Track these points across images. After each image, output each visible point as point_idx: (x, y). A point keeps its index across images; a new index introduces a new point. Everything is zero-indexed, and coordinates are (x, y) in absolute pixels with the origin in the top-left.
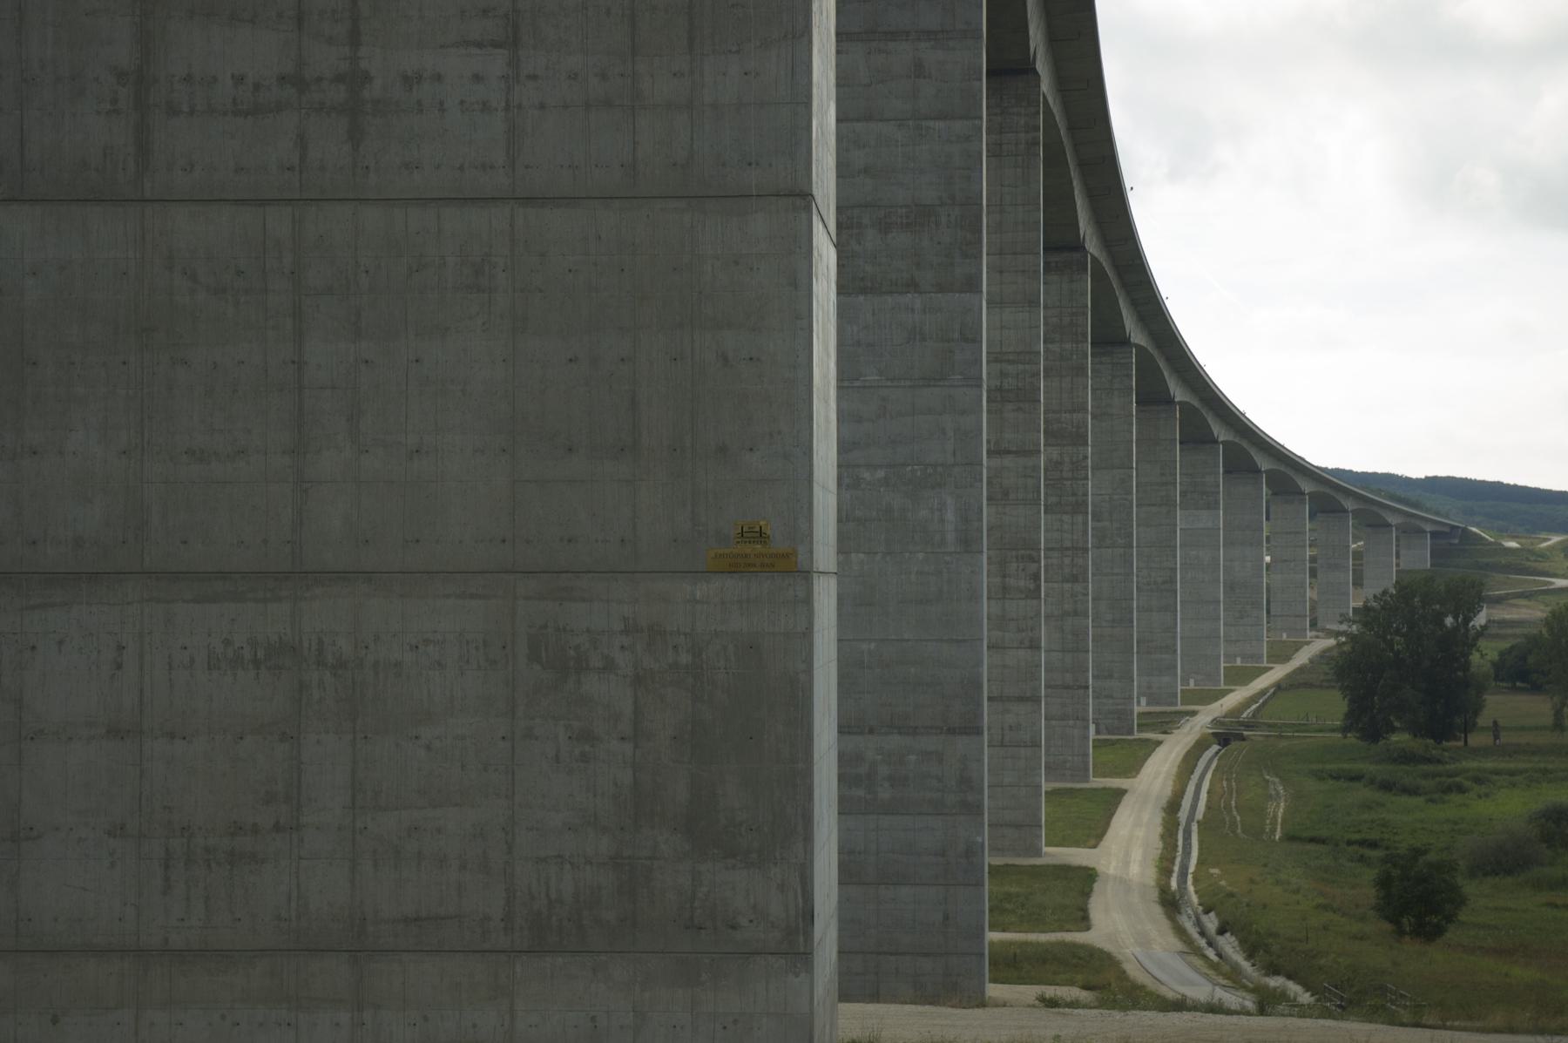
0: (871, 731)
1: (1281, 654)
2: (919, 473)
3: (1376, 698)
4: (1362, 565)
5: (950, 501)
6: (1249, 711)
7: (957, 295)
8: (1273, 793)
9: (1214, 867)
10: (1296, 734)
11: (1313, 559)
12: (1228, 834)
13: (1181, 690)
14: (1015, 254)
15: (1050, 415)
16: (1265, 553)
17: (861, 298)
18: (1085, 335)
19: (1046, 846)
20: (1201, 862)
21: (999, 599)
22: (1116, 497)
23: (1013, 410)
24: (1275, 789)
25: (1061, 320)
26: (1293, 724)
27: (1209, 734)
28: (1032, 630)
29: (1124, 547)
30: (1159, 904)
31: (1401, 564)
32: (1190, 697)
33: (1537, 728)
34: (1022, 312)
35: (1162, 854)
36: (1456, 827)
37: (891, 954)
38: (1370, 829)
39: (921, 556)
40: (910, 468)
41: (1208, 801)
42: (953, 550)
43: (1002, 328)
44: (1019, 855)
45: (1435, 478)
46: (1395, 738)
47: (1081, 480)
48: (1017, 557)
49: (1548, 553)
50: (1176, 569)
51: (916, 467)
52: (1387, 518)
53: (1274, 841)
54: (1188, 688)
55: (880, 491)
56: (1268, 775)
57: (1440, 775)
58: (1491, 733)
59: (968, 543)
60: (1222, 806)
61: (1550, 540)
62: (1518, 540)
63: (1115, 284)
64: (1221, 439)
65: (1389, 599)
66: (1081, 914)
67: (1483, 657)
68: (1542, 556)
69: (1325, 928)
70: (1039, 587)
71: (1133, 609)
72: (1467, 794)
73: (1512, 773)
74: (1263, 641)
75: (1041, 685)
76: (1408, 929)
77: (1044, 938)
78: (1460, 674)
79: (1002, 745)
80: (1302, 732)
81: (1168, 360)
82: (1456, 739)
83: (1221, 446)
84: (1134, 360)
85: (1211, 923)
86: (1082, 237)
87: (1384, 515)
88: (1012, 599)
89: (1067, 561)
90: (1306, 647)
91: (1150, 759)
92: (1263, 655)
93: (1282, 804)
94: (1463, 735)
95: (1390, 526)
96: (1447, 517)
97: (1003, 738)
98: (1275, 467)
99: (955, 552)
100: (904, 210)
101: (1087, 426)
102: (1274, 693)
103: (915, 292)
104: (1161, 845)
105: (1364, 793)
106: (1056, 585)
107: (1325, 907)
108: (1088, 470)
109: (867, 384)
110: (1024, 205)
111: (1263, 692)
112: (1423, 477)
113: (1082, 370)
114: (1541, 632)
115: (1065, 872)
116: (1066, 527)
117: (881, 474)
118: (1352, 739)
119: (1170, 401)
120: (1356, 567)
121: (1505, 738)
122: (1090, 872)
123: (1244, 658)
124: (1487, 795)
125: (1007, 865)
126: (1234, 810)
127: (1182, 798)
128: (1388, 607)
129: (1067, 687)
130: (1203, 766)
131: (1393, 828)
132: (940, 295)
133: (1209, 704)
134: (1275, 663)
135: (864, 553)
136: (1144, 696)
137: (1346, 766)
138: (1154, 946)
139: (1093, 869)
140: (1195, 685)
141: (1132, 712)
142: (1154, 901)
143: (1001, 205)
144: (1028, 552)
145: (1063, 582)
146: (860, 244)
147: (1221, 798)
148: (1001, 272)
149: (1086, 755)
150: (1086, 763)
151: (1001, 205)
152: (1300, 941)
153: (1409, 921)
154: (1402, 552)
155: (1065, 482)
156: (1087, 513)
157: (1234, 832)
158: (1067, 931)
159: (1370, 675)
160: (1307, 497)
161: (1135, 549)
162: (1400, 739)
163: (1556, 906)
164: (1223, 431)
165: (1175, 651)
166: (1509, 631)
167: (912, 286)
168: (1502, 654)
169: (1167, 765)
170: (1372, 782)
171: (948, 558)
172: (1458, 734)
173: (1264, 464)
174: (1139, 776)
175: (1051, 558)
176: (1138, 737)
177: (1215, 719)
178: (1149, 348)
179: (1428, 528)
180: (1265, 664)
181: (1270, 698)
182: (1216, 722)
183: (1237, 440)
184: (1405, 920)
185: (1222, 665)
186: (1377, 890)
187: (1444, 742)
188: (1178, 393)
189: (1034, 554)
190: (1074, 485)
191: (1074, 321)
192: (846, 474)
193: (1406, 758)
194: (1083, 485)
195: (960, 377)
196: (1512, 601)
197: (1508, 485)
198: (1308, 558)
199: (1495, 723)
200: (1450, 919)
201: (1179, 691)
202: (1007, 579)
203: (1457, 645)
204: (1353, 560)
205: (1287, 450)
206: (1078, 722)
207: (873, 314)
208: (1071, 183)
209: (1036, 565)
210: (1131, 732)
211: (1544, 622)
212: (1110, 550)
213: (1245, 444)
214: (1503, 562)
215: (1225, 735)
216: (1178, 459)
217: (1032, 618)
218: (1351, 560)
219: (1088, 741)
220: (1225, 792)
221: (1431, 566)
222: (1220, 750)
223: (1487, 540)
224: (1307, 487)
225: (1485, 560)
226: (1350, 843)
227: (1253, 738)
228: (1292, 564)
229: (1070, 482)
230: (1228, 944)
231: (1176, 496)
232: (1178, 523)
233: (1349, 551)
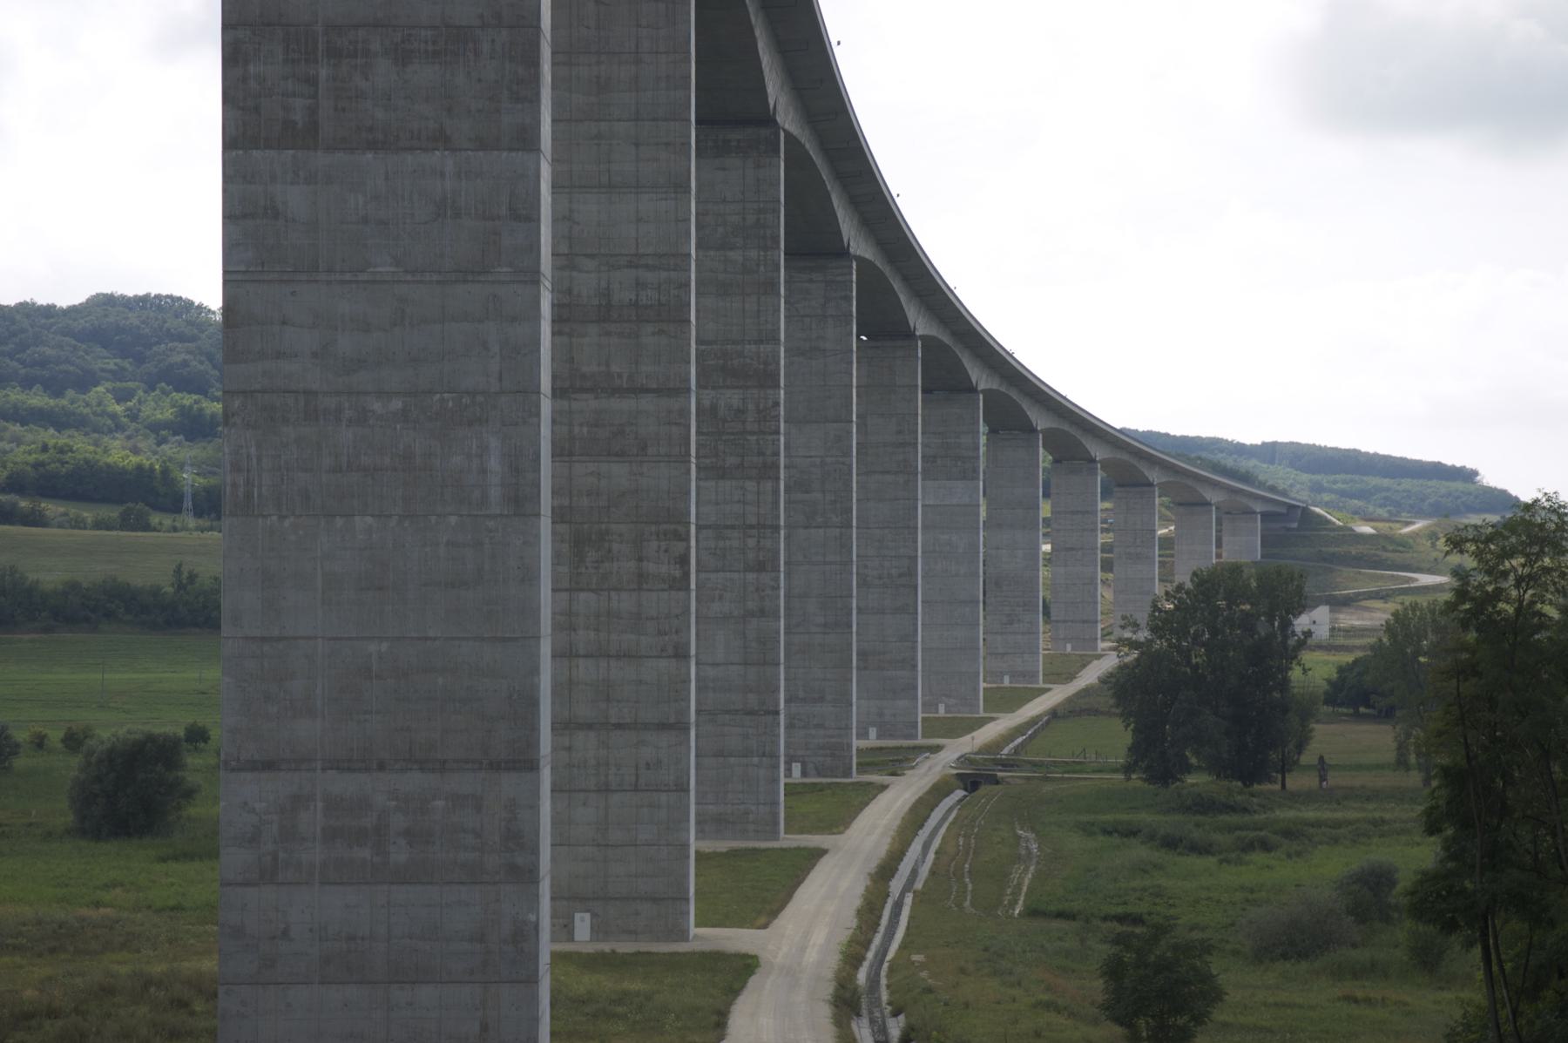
0: (382, 767)
1: (1061, 672)
2: (450, 404)
3: (1167, 727)
4: (1172, 556)
5: (494, 443)
6: (1011, 746)
12: (951, 907)
14: (654, 120)
16: (1041, 541)
17: (370, 156)
18: (776, 239)
19: (697, 925)
20: (904, 946)
21: (634, 590)
22: (829, 460)
23: (653, 334)
24: (1027, 848)
25: (744, 219)
27: (953, 775)
28: (677, 632)
30: (831, 1003)
31: (1224, 554)
32: (933, 727)
34: (666, 199)
36: (1250, 897)
38: (1140, 899)
39: (453, 520)
40: (438, 396)
41: (934, 864)
42: (498, 512)
43: (639, 220)
45: (1274, 444)
46: (1191, 779)
47: (771, 434)
49: (1411, 541)
51: (446, 395)
52: (1205, 495)
53: (1012, 917)
54: (936, 715)
55: (395, 428)
56: (1021, 830)
57: (1240, 828)
58: (1317, 774)
59: (521, 502)
60: (952, 869)
61: (1413, 523)
64: (981, 387)
65: (1185, 596)
66: (714, 1018)
68: (1403, 544)
70: (687, 575)
72: (1273, 854)
73: (1337, 825)
74: (1039, 653)
76: (1144, 1034)
79: (636, 790)
80: (1074, 772)
81: (905, 279)
82: (1271, 780)
89: (751, 542)
90: (1095, 662)
93: (1032, 868)
94: (1280, 776)
95: (1208, 504)
97: (637, 781)
99: (501, 515)
100: (429, 33)
102: (1048, 722)
103: (446, 149)
104: (854, 923)
105: (1139, 851)
106: (736, 576)
107: (1048, 1006)
111: (1033, 722)
112: (1259, 443)
113: (772, 286)
114: (1380, 640)
119: (909, 335)
120: (1165, 559)
121: (1334, 779)
122: (750, 961)
123: (1014, 675)
124: (1299, 854)
125: (639, 953)
126: (966, 875)
128: (1183, 607)
131: (1170, 898)
132: (481, 153)
135: (372, 516)
136: (875, 726)
137: (1124, 817)
140: (946, 712)
141: (850, 746)
144: (672, 527)
145: (745, 571)
146: (367, 79)
147: (952, 861)
148: (637, 145)
149: (776, 803)
150: (775, 815)
151: (637, 53)
153: (1147, 1023)
154: (1225, 539)
155: (749, 437)
156: (778, 479)
157: (960, 905)
161: (854, 530)
162: (1197, 781)
163: (1356, 1001)
164: (984, 376)
165: (915, 666)
167: (441, 140)
170: (1152, 837)
171: (491, 524)
173: (1041, 421)
176: (856, 780)
177: (962, 756)
179: (1258, 507)
180: (1041, 685)
181: (1042, 728)
182: (964, 760)
183: (1003, 389)
184: (1141, 1023)
185: (982, 685)
186: (1106, 982)
188: (921, 324)
189: (681, 529)
190: (761, 442)
192: (347, 405)
193: (1203, 805)
195: (509, 270)
196: (1368, 603)
197: (1367, 454)
198: (1099, 545)
199: (1321, 759)
201: (920, 720)
202: (645, 563)
204: (1159, 550)
205: (1071, 402)
206: (764, 759)
207: (387, 178)
210: (848, 774)
211: (1384, 628)
212: (821, 531)
213: (1014, 394)
214: (1354, 553)
215: (972, 778)
216: (920, 412)
217: (677, 616)
218: (1157, 548)
220: (959, 851)
221: (1262, 557)
222: (965, 797)
223: (1334, 523)
224: (1099, 452)
225: (1332, 549)
226: (1105, 919)
229: (755, 438)
232: (920, 497)
233: (1154, 538)
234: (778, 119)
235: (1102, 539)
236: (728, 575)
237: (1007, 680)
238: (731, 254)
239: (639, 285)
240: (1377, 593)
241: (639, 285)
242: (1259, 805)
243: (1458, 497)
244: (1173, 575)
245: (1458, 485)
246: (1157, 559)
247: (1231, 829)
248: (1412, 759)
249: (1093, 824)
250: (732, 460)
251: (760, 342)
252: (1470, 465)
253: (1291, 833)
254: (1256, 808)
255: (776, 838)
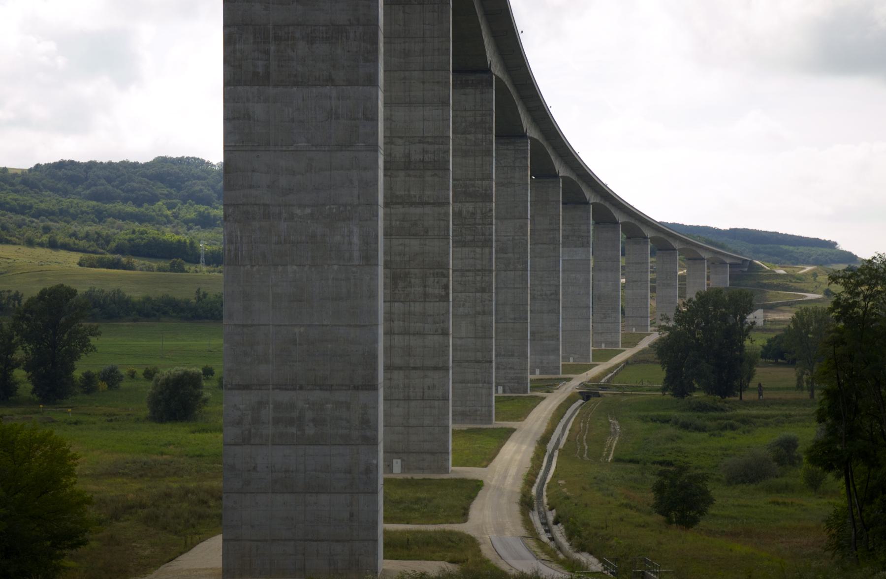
0: (301, 388)
1: (630, 342)
2: (334, 210)
3: (683, 369)
5: (356, 230)
7: (361, 88)
8: (612, 430)
9: (561, 480)
10: (633, 393)
11: (653, 281)
13: (562, 365)
15: (468, 182)
16: (620, 278)
17: (295, 89)
19: (453, 466)
21: (422, 301)
22: (516, 237)
23: (432, 176)
24: (614, 428)
26: (633, 386)
27: (577, 392)
28: (443, 322)
29: (522, 271)
33: (787, 388)
34: (438, 109)
35: (529, 471)
36: (725, 452)
37: (314, 541)
40: (328, 207)
43: (424, 120)
44: (434, 473)
45: (736, 230)
46: (695, 395)
47: (488, 225)
48: (433, 274)
50: (559, 285)
51: (332, 206)
57: (720, 419)
58: (757, 392)
59: (369, 259)
61: (805, 268)
62: (785, 269)
63: (515, 96)
64: (591, 201)
65: (692, 304)
66: (463, 511)
67: (756, 343)
68: (800, 279)
69: (622, 519)
70: (448, 294)
71: (527, 311)
72: (736, 431)
75: (449, 359)
77: (431, 528)
78: (738, 353)
79: (423, 399)
80: (637, 391)
81: (554, 149)
82: (735, 395)
83: (591, 206)
84: (529, 148)
85: (551, 516)
86: (489, 63)
87: (698, 251)
88: (430, 302)
89: (478, 278)
90: (647, 337)
91: (535, 409)
92: (619, 342)
93: (617, 438)
94: (739, 393)
95: (703, 259)
96: (741, 254)
97: (423, 395)
98: (627, 220)
99: (359, 265)
100: (324, 28)
101: (492, 190)
102: (624, 366)
103: (332, 85)
104: (530, 465)
106: (471, 294)
107: (627, 506)
108: (492, 219)
109: (299, 149)
110: (438, 37)
111: (617, 366)
113: (488, 152)
114: (789, 326)
115: (462, 483)
116: (478, 256)
117: (308, 211)
118: (668, 395)
119: (556, 176)
121: (766, 395)
122: (479, 483)
123: (607, 344)
124: (749, 432)
125: (424, 479)
126: (585, 441)
127: (553, 434)
129: (478, 362)
130: (569, 415)
131: (685, 453)
132: (349, 87)
133: (581, 373)
134: (627, 347)
135: (296, 265)
136: (538, 368)
137: (662, 413)
138: (506, 533)
139: (482, 481)
141: (526, 378)
142: (516, 503)
143: (424, 37)
145: (476, 292)
146: (294, 51)
148: (424, 83)
149: (490, 406)
150: (490, 412)
151: (424, 37)
152: (603, 528)
153: (676, 514)
155: (477, 226)
157: (582, 457)
158: (451, 523)
159: (680, 354)
160: (649, 240)
162: (698, 396)
163: (778, 503)
164: (593, 196)
165: (558, 339)
166: (777, 327)
167: (330, 81)
168: (769, 341)
169: (546, 413)
170: (676, 423)
171: (354, 269)
172: (736, 392)
173: (620, 218)
174: (526, 420)
175: (468, 276)
177: (581, 383)
178: (540, 140)
179: (728, 261)
180: (620, 348)
181: (621, 369)
182: (583, 385)
183: (602, 202)
185: (591, 348)
187: (727, 398)
188: (562, 171)
189: (445, 271)
191: (484, 120)
193: (701, 408)
194: (489, 228)
198: (649, 280)
199: (760, 385)
200: (701, 513)
201: (561, 365)
202: (427, 289)
203: (740, 332)
204: (679, 281)
206: (485, 384)
207: (303, 100)
208: (480, 26)
209: (446, 279)
210: (526, 392)
212: (512, 273)
213: (607, 205)
215: (587, 394)
217: (443, 314)
218: (678, 281)
219: (492, 398)
221: (730, 285)
222: (583, 403)
223: (765, 269)
225: (765, 281)
226: (654, 463)
227: (605, 395)
228: (639, 283)
229: (480, 227)
230: (559, 531)
231: (560, 238)
232: (561, 256)
233: (676, 276)
234: (492, 69)
235: (650, 276)
236: (467, 294)
237: (603, 345)
238: (468, 136)
239: (425, 152)
240: (787, 303)
241: (425, 152)
242: (729, 407)
243: (826, 256)
244: (685, 294)
245: (827, 250)
246: (678, 286)
247: (716, 419)
248: (805, 385)
249: (647, 417)
250: (469, 238)
251: (482, 179)
252: (833, 240)
253: (745, 421)
254: (727, 409)
255: (491, 423)
